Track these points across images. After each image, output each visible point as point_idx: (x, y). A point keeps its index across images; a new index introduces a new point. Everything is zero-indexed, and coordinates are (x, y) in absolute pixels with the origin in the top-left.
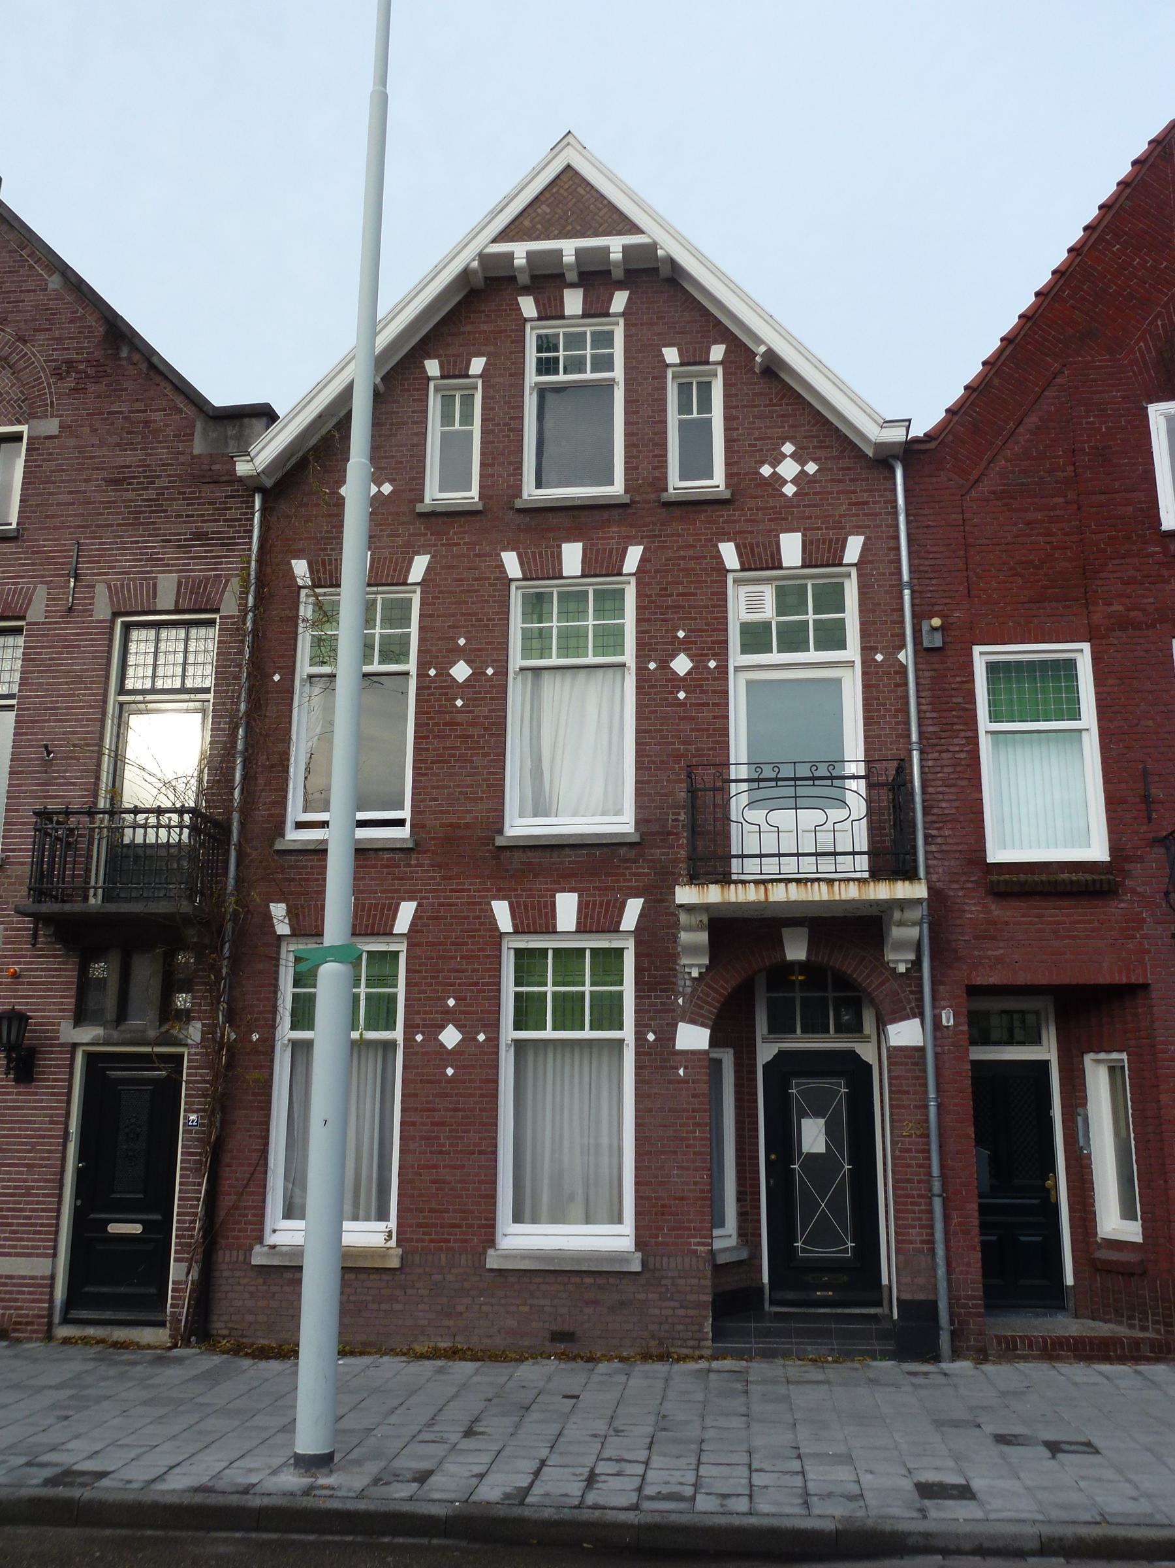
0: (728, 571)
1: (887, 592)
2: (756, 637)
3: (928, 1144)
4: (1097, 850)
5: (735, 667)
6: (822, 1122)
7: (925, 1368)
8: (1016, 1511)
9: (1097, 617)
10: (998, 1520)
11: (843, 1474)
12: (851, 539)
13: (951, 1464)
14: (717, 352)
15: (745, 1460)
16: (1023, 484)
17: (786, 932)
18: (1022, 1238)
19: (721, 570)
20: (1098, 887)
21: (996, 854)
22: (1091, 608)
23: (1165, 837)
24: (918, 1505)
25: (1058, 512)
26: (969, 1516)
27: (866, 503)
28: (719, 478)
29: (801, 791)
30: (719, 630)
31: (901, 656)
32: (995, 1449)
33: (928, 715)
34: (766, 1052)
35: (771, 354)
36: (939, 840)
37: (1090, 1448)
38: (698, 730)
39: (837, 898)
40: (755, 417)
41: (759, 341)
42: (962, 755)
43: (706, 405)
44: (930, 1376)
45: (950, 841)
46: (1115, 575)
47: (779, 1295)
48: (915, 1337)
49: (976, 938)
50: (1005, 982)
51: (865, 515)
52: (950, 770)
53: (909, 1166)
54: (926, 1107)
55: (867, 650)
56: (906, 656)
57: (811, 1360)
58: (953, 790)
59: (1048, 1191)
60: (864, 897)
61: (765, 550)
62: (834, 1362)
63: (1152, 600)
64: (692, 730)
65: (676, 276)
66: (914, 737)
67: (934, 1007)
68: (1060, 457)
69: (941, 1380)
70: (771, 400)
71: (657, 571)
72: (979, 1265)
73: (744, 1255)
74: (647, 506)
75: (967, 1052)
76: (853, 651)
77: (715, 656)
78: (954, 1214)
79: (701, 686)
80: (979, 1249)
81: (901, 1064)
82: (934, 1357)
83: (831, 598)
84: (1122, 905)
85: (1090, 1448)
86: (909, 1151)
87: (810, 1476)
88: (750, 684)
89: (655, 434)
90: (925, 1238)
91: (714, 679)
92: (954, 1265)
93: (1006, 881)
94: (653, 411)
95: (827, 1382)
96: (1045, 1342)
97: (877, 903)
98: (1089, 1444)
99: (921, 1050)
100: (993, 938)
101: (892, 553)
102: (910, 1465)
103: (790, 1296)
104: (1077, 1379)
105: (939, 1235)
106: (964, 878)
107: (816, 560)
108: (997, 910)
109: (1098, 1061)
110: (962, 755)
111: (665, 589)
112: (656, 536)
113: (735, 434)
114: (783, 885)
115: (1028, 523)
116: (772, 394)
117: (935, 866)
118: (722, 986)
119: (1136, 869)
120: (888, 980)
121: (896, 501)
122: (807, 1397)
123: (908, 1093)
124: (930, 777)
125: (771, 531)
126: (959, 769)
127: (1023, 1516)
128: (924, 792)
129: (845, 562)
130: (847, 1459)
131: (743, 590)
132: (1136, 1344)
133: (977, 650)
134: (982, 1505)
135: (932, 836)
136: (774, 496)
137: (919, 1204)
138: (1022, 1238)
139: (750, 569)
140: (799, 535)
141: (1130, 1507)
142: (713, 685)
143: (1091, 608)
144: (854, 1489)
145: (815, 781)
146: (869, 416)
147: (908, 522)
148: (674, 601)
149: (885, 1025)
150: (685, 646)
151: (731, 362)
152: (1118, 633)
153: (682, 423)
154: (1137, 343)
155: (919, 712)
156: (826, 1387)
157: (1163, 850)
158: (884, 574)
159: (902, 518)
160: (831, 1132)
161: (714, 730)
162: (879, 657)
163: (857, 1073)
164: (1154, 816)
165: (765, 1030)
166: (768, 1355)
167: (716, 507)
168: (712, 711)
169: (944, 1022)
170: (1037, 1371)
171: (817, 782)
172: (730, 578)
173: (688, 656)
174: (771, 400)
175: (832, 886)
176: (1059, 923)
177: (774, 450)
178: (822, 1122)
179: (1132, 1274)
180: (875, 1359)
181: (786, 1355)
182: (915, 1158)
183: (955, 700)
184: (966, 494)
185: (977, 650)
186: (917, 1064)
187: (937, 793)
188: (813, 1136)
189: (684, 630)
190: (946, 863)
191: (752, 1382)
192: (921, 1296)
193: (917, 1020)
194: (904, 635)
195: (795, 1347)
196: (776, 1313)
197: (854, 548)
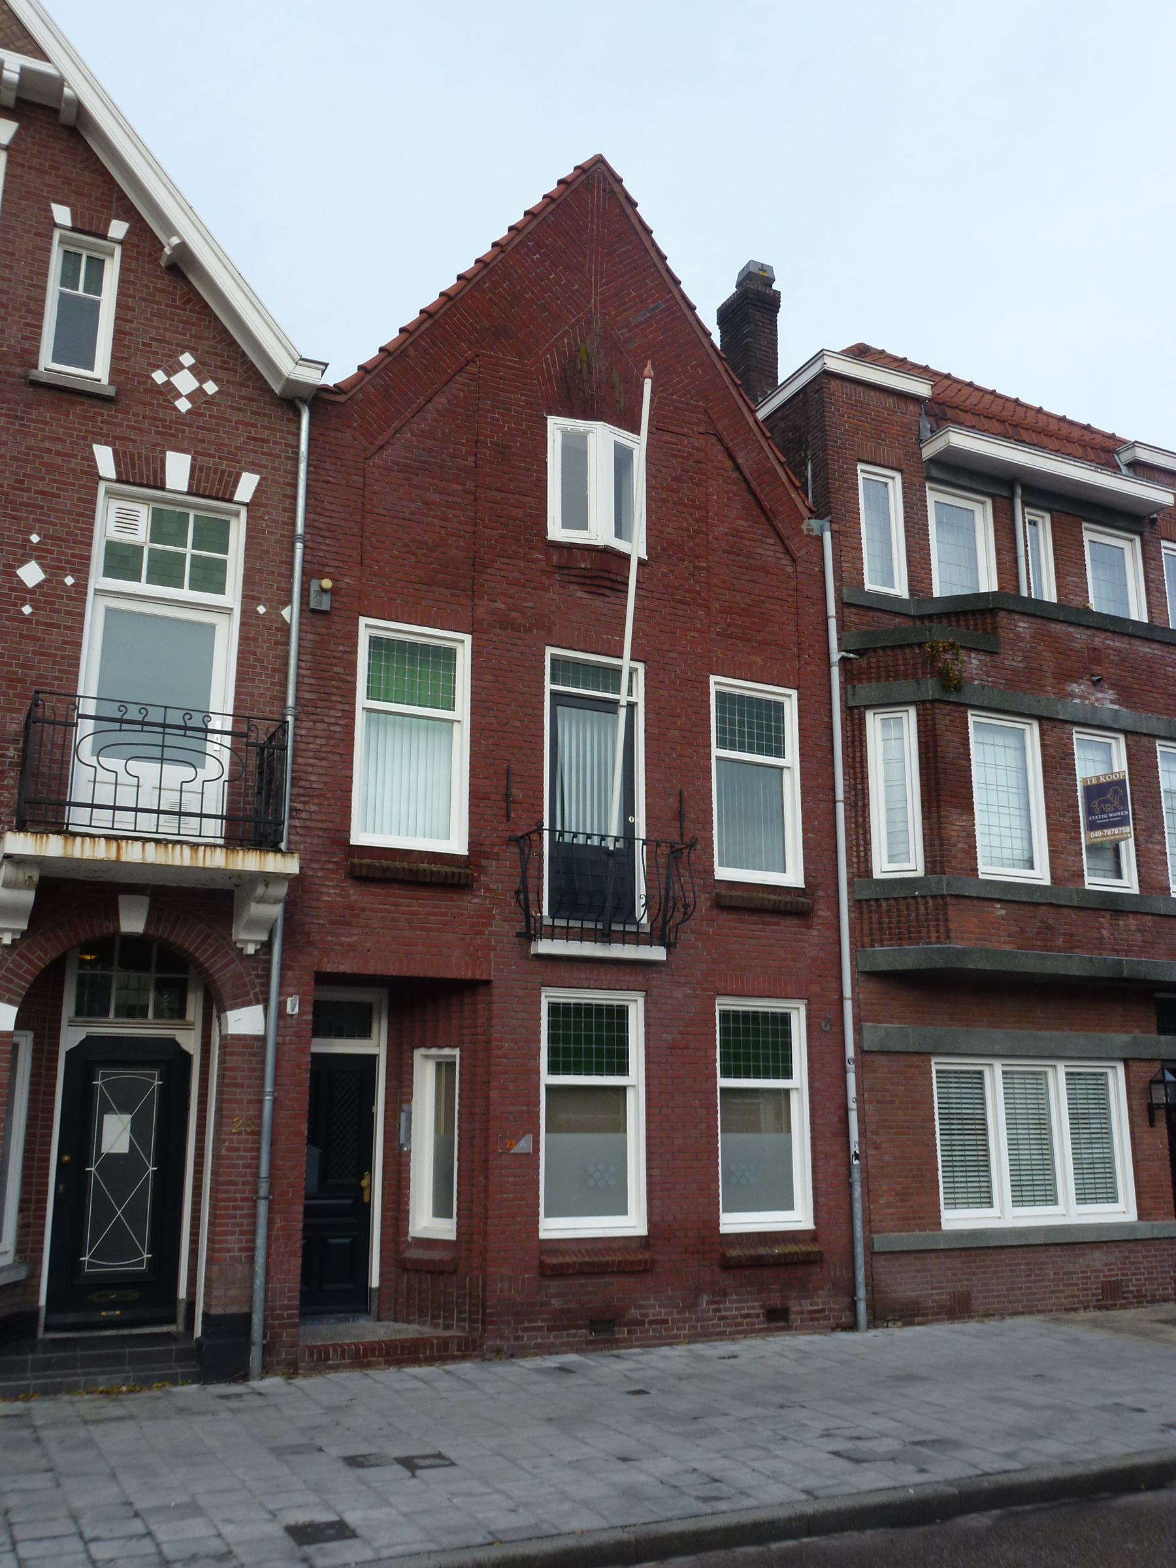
0: (101, 478)
1: (277, 541)
2: (122, 561)
3: (259, 1142)
4: (457, 844)
5: (96, 590)
6: (127, 1118)
7: (234, 1389)
8: (406, 1543)
9: (481, 612)
10: (391, 1558)
11: (197, 1528)
12: (245, 475)
13: (312, 1498)
14: (118, 229)
15: (72, 1529)
16: (426, 463)
17: (123, 900)
18: (332, 1241)
19: (94, 476)
20: (456, 880)
21: (359, 837)
22: (476, 601)
23: (522, 837)
24: (299, 1554)
25: (456, 499)
26: (358, 1559)
27: (267, 442)
28: (101, 371)
29: (169, 740)
30: (81, 543)
31: (285, 613)
32: (352, 1474)
33: (307, 680)
34: (71, 1037)
35: (183, 249)
36: (304, 815)
37: (441, 1460)
38: (43, 654)
39: (200, 864)
40: (153, 314)
41: (171, 230)
42: (337, 729)
43: (95, 284)
44: (245, 1397)
45: (314, 817)
46: (502, 573)
47: (57, 1319)
48: (222, 1355)
49: (331, 922)
50: (355, 970)
51: (263, 453)
52: (323, 742)
53: (235, 1166)
54: (261, 1102)
55: (249, 599)
56: (291, 614)
57: (102, 1392)
58: (324, 763)
59: (362, 1190)
60: (230, 867)
61: (148, 464)
62: (130, 1392)
63: (531, 604)
64: (35, 653)
65: (80, 129)
66: (291, 702)
67: (280, 994)
68: (463, 445)
69: (259, 1401)
70: (174, 301)
71: (13, 459)
72: (299, 1271)
73: (22, 1274)
74: (10, 379)
75: (309, 1043)
76: (232, 596)
77: (73, 572)
78: (278, 1218)
79: (53, 603)
80: (300, 1254)
81: (238, 1054)
82: (240, 1374)
83: (214, 535)
84: (475, 901)
85: (441, 1460)
86: (237, 1149)
87: (161, 1537)
88: (109, 611)
89: (32, 299)
90: (244, 1245)
91: (70, 598)
92: (272, 1274)
93: (368, 866)
94: (31, 272)
95: (131, 1417)
96: (358, 1349)
97: (240, 875)
98: (439, 1456)
99: (262, 1039)
100: (349, 924)
101: (288, 501)
102: (271, 1507)
103: (70, 1318)
104: (398, 1386)
105: (261, 1242)
106: (324, 859)
107: (205, 488)
108: (355, 894)
109: (427, 1057)
110: (337, 729)
111: (21, 482)
112: (16, 417)
113: (128, 327)
114: (139, 844)
115: (426, 503)
116: (174, 292)
117: (296, 843)
118: (39, 958)
119: (492, 865)
120: (233, 961)
121: (298, 447)
122: (116, 1438)
123: (242, 1086)
124: (303, 746)
125: (157, 445)
126: (332, 742)
127: (415, 1547)
128: (294, 763)
129: (236, 498)
130: (193, 1509)
131: (115, 504)
132: (445, 1343)
133: (363, 621)
134: (367, 1542)
135: (297, 810)
136: (165, 407)
137: (241, 1208)
138: (332, 1241)
139: (127, 482)
140: (189, 457)
141: (514, 1521)
142: (67, 605)
143: (476, 601)
144: (215, 1545)
145: (167, 731)
146: (285, 348)
147: (308, 473)
148: (30, 498)
149: (223, 1010)
150: (38, 554)
151: (133, 245)
152: (499, 631)
153: (63, 297)
154: (544, 354)
155: (298, 675)
156: (132, 1423)
157: (517, 850)
158: (276, 521)
159: (303, 467)
160: (137, 1129)
161: (63, 657)
162: (261, 609)
163: (174, 1063)
164: (513, 815)
165: (72, 1014)
166: (49, 1391)
167: (94, 402)
168: (61, 635)
169: (289, 1011)
170: (349, 1381)
171: (189, 733)
172: (102, 487)
173: (41, 565)
174: (174, 301)
175: (197, 850)
176: (415, 913)
177: (171, 357)
178: (127, 1118)
179: (441, 1273)
180: (175, 1384)
181: (71, 1389)
182: (242, 1158)
183: (336, 669)
184: (370, 458)
185: (363, 621)
186: (254, 1055)
187: (306, 765)
188: (116, 1134)
189: (39, 534)
190: (308, 841)
191: (41, 1427)
192: (234, 1310)
193: (260, 1007)
194: (290, 591)
195: (83, 1379)
196: (53, 1341)
197: (247, 486)
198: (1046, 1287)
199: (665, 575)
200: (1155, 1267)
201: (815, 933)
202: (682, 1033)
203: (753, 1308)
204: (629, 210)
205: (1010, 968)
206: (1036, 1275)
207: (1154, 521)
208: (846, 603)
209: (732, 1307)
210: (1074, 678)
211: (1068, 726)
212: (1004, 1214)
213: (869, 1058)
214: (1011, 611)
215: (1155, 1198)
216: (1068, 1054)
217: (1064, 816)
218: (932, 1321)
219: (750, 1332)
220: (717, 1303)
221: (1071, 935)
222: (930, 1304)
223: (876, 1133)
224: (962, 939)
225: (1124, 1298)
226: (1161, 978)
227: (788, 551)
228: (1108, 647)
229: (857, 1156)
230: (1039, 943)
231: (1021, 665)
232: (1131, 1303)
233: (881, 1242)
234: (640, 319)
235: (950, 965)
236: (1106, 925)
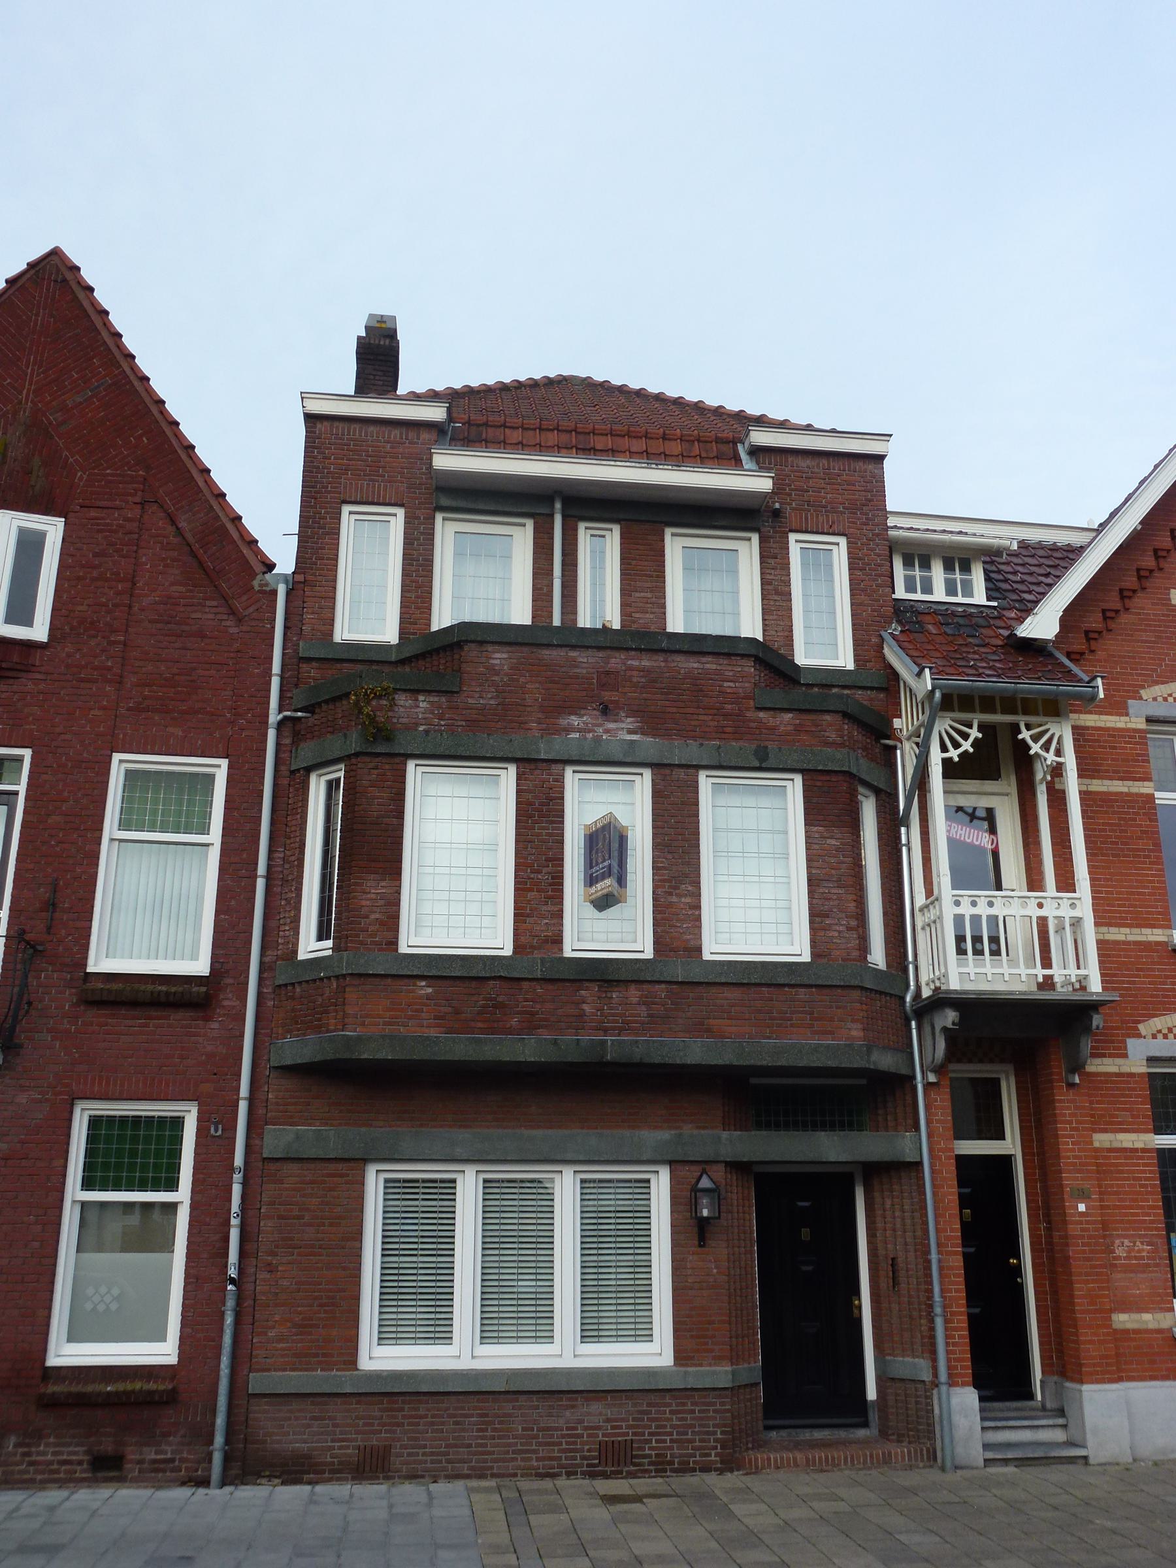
198: (509, 1445)
199: (69, 655)
200: (692, 1426)
201: (215, 1025)
202: (22, 1142)
203: (75, 1453)
204: (81, 295)
205: (426, 1056)
206: (495, 1430)
207: (776, 514)
208: (302, 658)
209: (46, 1452)
210: (575, 708)
211: (556, 768)
212: (464, 1350)
213: (273, 1166)
214: (482, 643)
215: (698, 1337)
216: (569, 1157)
217: (539, 872)
218: (329, 1480)
219: (69, 1481)
220: (28, 1445)
221: (533, 1014)
222: (329, 1459)
223: (273, 1254)
224: (363, 1024)
225: (635, 1465)
226: (449, 1057)
227: (232, 612)
228: (631, 668)
229: (232, 1281)
230: (480, 1025)
231: (492, 702)
232: (646, 1471)
233: (257, 1382)
234: (79, 399)
235: (338, 1056)
236: (590, 1000)
